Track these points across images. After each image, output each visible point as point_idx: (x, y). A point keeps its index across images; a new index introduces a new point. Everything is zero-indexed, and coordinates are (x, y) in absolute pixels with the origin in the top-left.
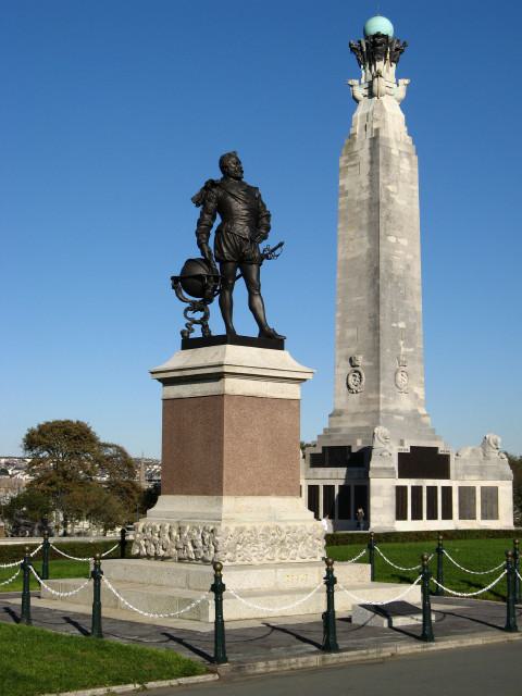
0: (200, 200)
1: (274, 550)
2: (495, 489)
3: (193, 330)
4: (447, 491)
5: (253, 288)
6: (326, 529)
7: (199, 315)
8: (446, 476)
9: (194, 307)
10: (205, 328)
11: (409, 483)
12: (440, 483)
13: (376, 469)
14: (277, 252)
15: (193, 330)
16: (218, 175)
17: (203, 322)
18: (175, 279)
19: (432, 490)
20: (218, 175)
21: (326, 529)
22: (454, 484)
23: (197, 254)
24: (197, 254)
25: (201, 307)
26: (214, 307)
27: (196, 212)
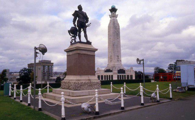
0: (73, 15)
1: (89, 87)
2: (132, 75)
3: (73, 41)
4: (125, 76)
5: (85, 32)
6: (13, 19)
7: (73, 38)
8: (125, 73)
9: (73, 37)
10: (75, 41)
11: (119, 74)
12: (124, 74)
13: (55, 65)
14: (90, 25)
15: (73, 41)
16: (77, 10)
17: (75, 40)
18: (69, 31)
19: (123, 76)
20: (77, 10)
21: (13, 19)
22: (126, 75)
23: (73, 26)
24: (73, 26)
25: (75, 37)
26: (77, 37)
27: (73, 17)
